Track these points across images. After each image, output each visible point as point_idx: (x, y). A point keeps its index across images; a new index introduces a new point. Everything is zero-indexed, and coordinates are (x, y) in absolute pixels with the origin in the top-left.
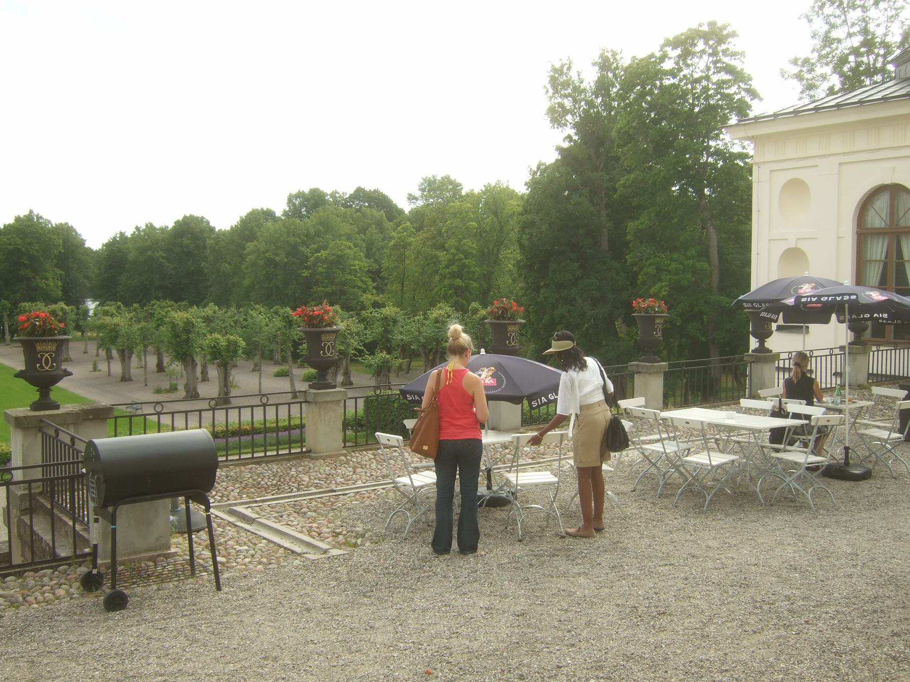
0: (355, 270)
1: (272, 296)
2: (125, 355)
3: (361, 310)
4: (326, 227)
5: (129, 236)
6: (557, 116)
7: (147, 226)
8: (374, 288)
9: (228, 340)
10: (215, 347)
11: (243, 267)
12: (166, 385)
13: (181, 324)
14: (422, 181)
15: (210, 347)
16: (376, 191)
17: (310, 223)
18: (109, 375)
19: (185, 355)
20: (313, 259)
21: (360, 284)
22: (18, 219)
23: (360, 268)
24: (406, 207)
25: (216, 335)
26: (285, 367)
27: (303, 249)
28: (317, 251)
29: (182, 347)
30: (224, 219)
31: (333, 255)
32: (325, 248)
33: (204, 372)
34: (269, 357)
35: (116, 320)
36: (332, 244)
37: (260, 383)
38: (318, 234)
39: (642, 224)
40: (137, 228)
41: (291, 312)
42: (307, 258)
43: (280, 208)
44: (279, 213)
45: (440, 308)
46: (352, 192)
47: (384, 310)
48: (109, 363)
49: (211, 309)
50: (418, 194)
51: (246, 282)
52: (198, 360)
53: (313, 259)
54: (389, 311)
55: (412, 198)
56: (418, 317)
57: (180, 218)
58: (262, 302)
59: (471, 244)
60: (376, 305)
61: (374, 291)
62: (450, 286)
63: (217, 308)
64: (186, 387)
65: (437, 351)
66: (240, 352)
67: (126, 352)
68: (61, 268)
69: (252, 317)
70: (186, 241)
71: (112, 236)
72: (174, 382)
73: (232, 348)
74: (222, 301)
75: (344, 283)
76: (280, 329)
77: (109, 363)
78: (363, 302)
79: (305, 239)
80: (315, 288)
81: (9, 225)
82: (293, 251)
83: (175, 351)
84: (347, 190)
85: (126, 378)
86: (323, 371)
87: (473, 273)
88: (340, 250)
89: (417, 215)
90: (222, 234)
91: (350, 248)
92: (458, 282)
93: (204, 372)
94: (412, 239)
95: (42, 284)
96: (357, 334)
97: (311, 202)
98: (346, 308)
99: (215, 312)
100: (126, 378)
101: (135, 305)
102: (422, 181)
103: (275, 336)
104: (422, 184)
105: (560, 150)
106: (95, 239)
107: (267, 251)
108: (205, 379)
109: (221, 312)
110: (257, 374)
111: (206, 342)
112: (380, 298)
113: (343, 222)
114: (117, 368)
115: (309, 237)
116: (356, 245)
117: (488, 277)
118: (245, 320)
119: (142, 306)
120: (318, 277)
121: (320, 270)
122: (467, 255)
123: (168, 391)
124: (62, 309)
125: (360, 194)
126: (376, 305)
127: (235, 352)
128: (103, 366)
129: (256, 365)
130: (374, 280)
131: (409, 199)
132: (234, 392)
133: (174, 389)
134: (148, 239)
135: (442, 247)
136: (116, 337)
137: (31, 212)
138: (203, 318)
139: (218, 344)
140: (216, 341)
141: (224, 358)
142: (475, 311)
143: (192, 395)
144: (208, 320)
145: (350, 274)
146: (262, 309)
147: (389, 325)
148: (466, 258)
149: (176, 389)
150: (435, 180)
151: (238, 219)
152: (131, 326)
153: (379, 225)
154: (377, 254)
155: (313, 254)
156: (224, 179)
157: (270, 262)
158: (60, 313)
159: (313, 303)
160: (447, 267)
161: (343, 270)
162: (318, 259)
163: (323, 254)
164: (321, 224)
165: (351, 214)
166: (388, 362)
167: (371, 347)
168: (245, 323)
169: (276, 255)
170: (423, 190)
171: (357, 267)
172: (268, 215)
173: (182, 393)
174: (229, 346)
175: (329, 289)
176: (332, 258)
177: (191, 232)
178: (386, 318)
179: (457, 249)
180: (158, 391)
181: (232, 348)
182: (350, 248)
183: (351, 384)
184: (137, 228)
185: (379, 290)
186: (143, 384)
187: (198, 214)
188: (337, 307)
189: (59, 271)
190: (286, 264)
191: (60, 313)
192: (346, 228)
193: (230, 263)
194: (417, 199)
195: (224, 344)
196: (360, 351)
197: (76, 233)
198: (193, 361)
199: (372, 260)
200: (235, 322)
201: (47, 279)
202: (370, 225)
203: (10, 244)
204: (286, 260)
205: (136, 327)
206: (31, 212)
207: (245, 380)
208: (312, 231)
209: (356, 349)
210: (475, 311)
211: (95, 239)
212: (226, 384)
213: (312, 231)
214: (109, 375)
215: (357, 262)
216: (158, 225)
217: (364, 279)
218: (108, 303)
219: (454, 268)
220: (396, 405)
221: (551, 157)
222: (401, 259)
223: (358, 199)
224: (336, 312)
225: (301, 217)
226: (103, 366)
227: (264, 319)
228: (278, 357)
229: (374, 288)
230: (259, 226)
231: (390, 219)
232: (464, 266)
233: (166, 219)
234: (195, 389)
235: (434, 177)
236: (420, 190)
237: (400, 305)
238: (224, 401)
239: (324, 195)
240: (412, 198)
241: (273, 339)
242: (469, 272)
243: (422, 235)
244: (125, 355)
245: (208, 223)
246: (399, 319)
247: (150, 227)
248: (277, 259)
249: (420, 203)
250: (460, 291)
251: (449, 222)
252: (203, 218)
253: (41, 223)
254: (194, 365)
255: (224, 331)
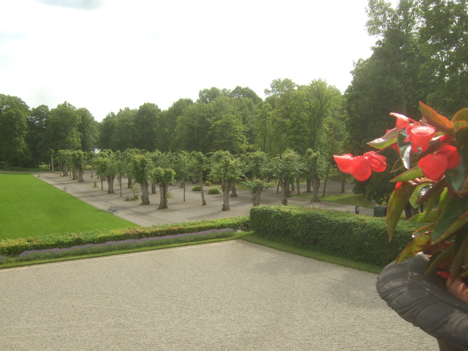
0: (237, 131)
1: (192, 145)
2: (110, 179)
3: (240, 153)
4: (220, 107)
5: (116, 115)
6: (373, 28)
7: (125, 109)
8: (247, 141)
9: (166, 171)
10: (158, 175)
11: (175, 130)
12: (132, 195)
13: (139, 162)
14: (272, 82)
15: (155, 175)
16: (247, 88)
17: (212, 105)
18: (102, 189)
19: (141, 179)
20: (213, 125)
21: (239, 138)
22: (59, 106)
23: (240, 130)
24: (263, 97)
25: (159, 168)
26: (198, 186)
27: (208, 119)
28: (216, 120)
29: (139, 174)
30: (164, 105)
31: (225, 122)
32: (220, 119)
33: (153, 189)
34: (191, 180)
35: (105, 159)
36: (224, 116)
37: (184, 196)
38: (216, 111)
39: (438, 94)
40: (121, 110)
41: (202, 155)
42: (210, 125)
43: (195, 98)
44: (194, 101)
45: (288, 152)
46: (234, 89)
47: (256, 153)
48: (102, 183)
49: (157, 153)
50: (270, 89)
51: (177, 138)
52: (150, 182)
53: (213, 125)
54: (259, 154)
55: (267, 91)
56: (277, 157)
57: (142, 104)
58: (185, 149)
59: (305, 115)
60: (249, 150)
61: (248, 143)
62: (293, 139)
63: (160, 152)
64: (143, 197)
65: (288, 177)
66: (173, 178)
67: (111, 177)
68: (81, 132)
69: (180, 158)
70: (145, 117)
71: (107, 114)
72: (136, 194)
73: (168, 175)
74: (164, 149)
75: (231, 138)
76: (195, 164)
77: (102, 183)
78: (241, 149)
79: (209, 114)
80: (215, 141)
81: (54, 109)
82: (202, 121)
83: (136, 177)
84: (231, 87)
85: (111, 192)
86: (212, 176)
87: (307, 131)
88: (228, 120)
89: (270, 100)
90: (164, 112)
91: (234, 119)
92: (298, 137)
93: (153, 189)
94: (270, 112)
95: (71, 139)
96: (241, 167)
97: (212, 94)
98: (233, 152)
99: (159, 155)
100: (111, 192)
101: (118, 151)
102: (272, 82)
103: (193, 168)
104: (272, 84)
105: (373, 48)
106: (99, 117)
107: (188, 121)
108: (154, 192)
109: (162, 155)
110: (183, 189)
111: (153, 172)
112: (251, 146)
113: (230, 104)
114: (106, 185)
115: (211, 114)
116: (237, 117)
117: (314, 134)
118: (176, 159)
119: (122, 152)
120: (216, 135)
121: (218, 131)
122: (303, 121)
123: (133, 200)
124: (79, 154)
125: (238, 90)
126: (249, 150)
127: (170, 178)
128: (99, 184)
129: (182, 184)
130: (247, 137)
131: (265, 92)
132: (169, 201)
133: (136, 198)
134: (125, 115)
135: (288, 116)
136: (105, 169)
137: (65, 102)
138: (153, 158)
139: (160, 173)
140: (159, 171)
141: (163, 182)
142: (310, 154)
143: (146, 202)
144: (155, 159)
145: (234, 133)
146: (186, 153)
147: (259, 162)
148: (302, 123)
149: (137, 198)
150: (280, 81)
151: (173, 104)
152: (113, 162)
153: (249, 106)
154: (249, 122)
155: (213, 122)
156: (165, 83)
157: (191, 127)
158: (78, 156)
159: (213, 150)
160: (291, 128)
161: (230, 131)
162: (216, 125)
163: (219, 122)
164: (218, 105)
165: (234, 101)
166: (260, 185)
167: (249, 175)
168: (176, 161)
169: (193, 123)
170: (273, 87)
171: (238, 129)
172: (189, 102)
173: (140, 201)
174: (166, 174)
175: (222, 142)
176: (224, 124)
177: (147, 113)
178: (257, 158)
179: (297, 117)
180: (127, 200)
181: (168, 176)
182: (234, 119)
183: (236, 196)
184: (121, 110)
185: (251, 142)
186: (120, 196)
187: (151, 102)
188: (228, 152)
189: (80, 134)
190: (198, 128)
191: (78, 156)
192: (231, 108)
193: (168, 128)
194: (270, 92)
195: (163, 173)
196: (243, 178)
197: (89, 113)
198: (146, 183)
199: (246, 125)
200: (171, 161)
201: (73, 137)
202: (244, 106)
203: (54, 119)
204: (198, 126)
205: (116, 163)
206: (65, 102)
207: (175, 193)
208: (213, 110)
209: (241, 177)
210: (310, 154)
211: (99, 117)
212: (165, 196)
213: (213, 110)
214: (102, 189)
215: (238, 127)
216: (131, 109)
217: (242, 136)
218: (104, 150)
219: (296, 129)
220: (272, 216)
221: (368, 54)
222: (264, 124)
223: (237, 93)
224: (227, 155)
225: (207, 103)
226: (99, 184)
227: (187, 159)
228: (194, 179)
229: (247, 141)
230: (184, 107)
231: (256, 103)
232: (301, 127)
233: (135, 106)
234: (147, 199)
235: (279, 79)
236: (271, 87)
237: (263, 150)
238: (163, 206)
239: (220, 91)
240: (267, 91)
241: (191, 170)
242: (304, 131)
243: (275, 111)
244: (110, 179)
245: (157, 107)
246: (265, 158)
247: (127, 109)
248: (194, 125)
249: (271, 94)
250: (298, 142)
251: (292, 102)
252: (154, 104)
253: (70, 108)
254: (147, 185)
255: (164, 166)
